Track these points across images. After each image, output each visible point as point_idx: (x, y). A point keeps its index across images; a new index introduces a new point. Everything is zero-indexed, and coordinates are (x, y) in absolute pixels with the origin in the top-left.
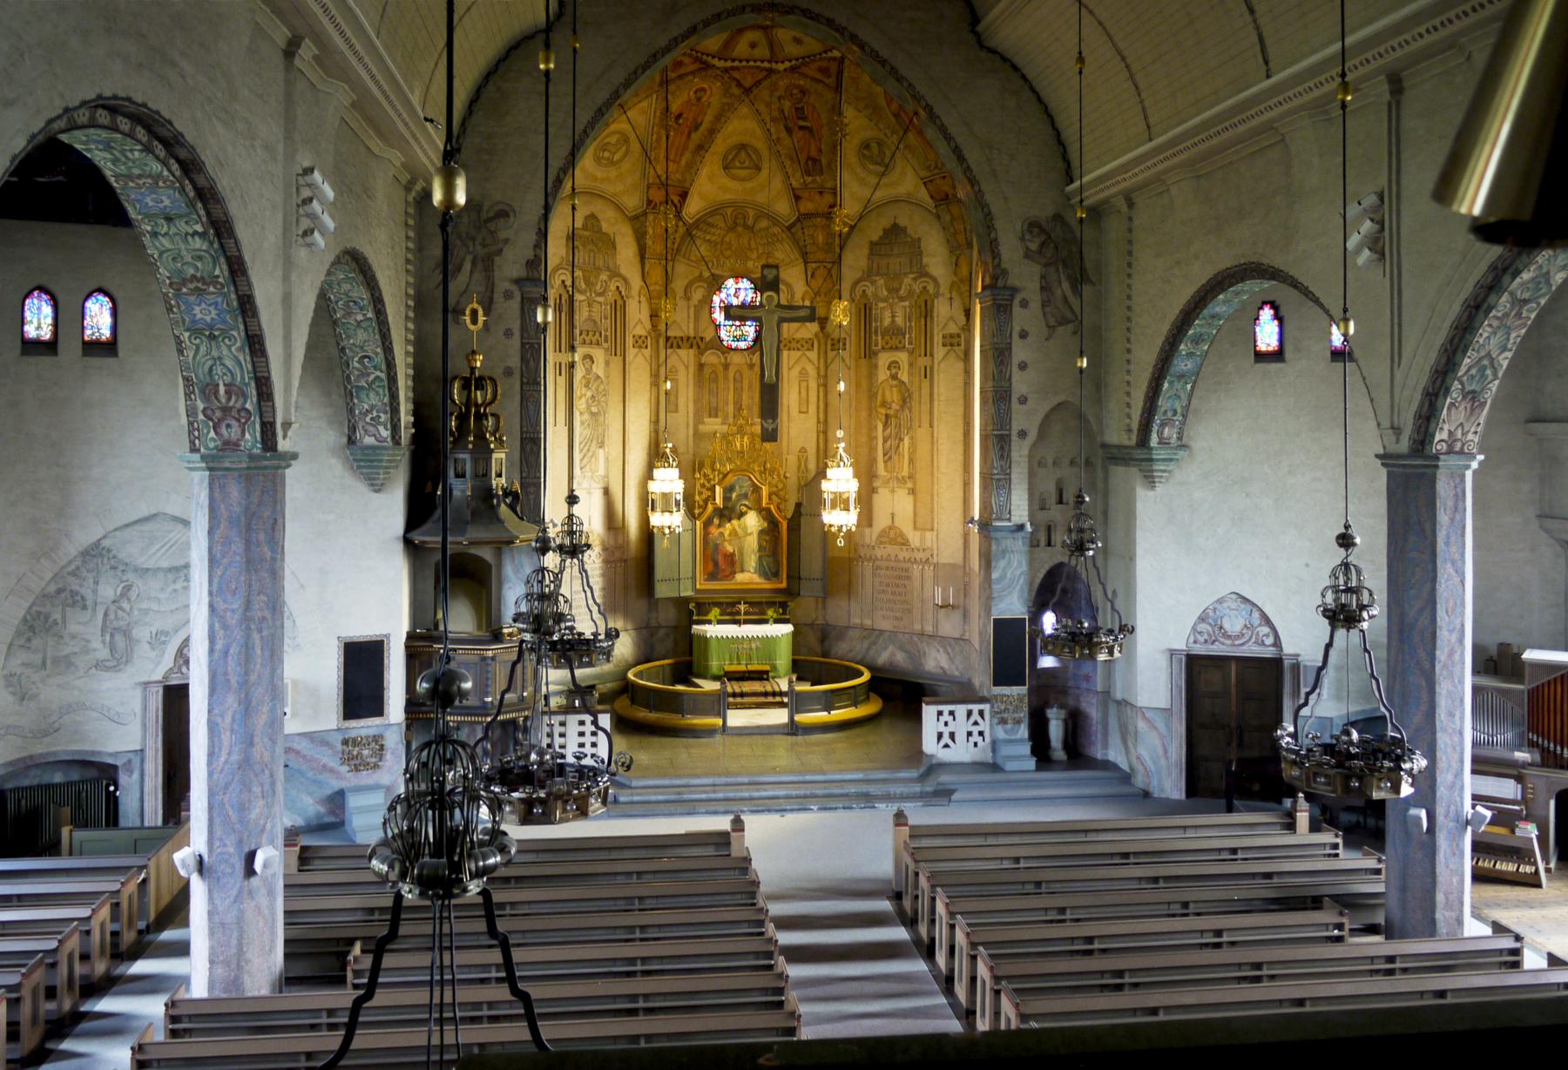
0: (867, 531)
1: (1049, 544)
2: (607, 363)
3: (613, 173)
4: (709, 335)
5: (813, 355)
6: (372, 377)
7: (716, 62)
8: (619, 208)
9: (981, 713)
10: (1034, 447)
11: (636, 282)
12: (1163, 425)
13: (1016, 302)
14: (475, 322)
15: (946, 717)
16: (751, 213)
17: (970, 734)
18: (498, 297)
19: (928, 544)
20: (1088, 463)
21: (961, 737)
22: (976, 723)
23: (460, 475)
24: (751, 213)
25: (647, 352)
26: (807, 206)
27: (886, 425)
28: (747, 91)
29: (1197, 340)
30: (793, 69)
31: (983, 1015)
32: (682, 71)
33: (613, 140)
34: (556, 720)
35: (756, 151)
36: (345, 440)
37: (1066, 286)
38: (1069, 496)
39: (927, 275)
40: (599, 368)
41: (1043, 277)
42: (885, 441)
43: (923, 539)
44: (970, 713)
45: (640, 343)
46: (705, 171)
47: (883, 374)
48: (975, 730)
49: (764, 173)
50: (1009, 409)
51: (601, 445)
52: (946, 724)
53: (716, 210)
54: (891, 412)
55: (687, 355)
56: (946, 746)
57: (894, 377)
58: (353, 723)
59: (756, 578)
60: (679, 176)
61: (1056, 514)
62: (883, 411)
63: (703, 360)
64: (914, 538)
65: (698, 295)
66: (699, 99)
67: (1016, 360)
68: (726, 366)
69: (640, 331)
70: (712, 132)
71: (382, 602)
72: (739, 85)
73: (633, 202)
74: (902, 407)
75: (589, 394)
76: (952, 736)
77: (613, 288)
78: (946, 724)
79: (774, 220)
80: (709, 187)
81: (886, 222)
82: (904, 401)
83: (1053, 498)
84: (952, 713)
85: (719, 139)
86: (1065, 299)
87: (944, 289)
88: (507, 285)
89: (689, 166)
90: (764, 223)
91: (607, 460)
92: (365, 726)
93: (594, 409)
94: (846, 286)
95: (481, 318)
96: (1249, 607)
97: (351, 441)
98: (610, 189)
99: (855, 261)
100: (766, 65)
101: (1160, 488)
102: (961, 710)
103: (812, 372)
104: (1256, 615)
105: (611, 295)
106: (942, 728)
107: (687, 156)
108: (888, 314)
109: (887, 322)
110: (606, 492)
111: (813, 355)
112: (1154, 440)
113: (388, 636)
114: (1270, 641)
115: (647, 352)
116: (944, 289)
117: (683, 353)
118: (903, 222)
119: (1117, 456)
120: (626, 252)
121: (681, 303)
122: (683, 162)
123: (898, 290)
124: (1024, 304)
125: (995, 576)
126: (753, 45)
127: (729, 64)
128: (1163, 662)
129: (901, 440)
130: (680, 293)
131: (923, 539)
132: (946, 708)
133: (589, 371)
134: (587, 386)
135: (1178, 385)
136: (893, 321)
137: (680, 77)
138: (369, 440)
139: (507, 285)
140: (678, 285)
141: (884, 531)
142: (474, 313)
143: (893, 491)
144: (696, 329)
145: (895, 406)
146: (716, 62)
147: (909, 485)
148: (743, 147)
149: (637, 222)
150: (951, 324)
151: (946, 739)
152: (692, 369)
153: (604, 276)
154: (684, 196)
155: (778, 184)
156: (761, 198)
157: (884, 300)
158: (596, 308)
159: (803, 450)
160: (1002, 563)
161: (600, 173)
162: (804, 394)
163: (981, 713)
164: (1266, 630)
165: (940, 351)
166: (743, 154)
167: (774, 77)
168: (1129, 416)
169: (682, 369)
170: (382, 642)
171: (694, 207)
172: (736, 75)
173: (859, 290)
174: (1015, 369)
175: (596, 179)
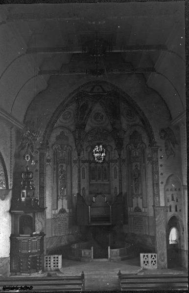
0: (132, 208)
4: (92, 159)
8: (69, 130)
9: (155, 256)
10: (165, 186)
13: (159, 150)
14: (28, 159)
15: (146, 257)
17: (152, 261)
20: (179, 189)
21: (150, 262)
22: (153, 259)
23: (23, 196)
25: (77, 164)
27: (135, 181)
33: (67, 113)
38: (175, 199)
39: (143, 143)
40: (64, 168)
41: (165, 143)
43: (145, 210)
44: (152, 256)
45: (75, 162)
47: (134, 168)
48: (154, 260)
50: (158, 177)
52: (146, 259)
56: (146, 265)
61: (171, 203)
65: (89, 149)
67: (159, 164)
75: (62, 175)
76: (148, 262)
78: (146, 259)
79: (69, 130)
83: (170, 199)
84: (147, 256)
86: (171, 148)
91: (67, 191)
94: (124, 146)
95: (29, 158)
102: (150, 255)
103: (117, 168)
106: (145, 260)
109: (134, 155)
115: (77, 164)
116: (147, 146)
117: (86, 164)
121: (85, 152)
123: (136, 147)
124: (161, 150)
126: (98, 89)
127: (93, 94)
130: (85, 149)
131: (145, 210)
132: (146, 255)
134: (62, 173)
136: (136, 155)
140: (84, 147)
142: (28, 157)
144: (89, 158)
147: (141, 196)
151: (146, 263)
153: (66, 146)
158: (63, 153)
159: (116, 188)
161: (64, 121)
163: (155, 256)
165: (147, 162)
174: (159, 166)
175: (63, 123)
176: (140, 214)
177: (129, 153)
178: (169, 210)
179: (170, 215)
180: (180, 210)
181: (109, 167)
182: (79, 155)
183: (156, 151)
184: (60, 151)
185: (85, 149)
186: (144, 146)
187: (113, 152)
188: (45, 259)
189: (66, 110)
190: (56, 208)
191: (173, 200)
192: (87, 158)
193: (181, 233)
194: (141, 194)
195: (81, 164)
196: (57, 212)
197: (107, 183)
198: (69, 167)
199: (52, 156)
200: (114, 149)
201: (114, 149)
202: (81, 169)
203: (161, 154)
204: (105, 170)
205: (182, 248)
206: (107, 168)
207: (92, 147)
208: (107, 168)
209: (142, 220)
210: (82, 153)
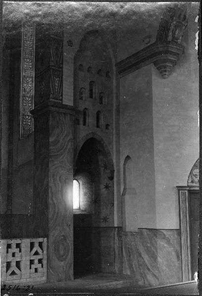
1: (84, 124)
12: (176, 27)
22: (36, 253)
44: (32, 245)
52: (14, 255)
78: (14, 255)
83: (86, 94)
84: (18, 246)
128: (174, 197)
160: (57, 131)
163: (40, 244)
178: (81, 122)
179: (84, 133)
180: (107, 126)
191: (91, 96)
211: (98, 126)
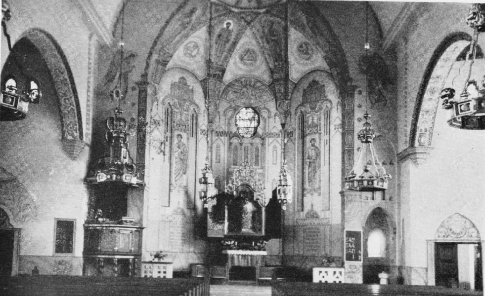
0: (301, 213)
2: (188, 139)
3: (192, 61)
5: (279, 140)
6: (69, 109)
7: (233, 9)
9: (341, 273)
11: (203, 107)
13: (356, 92)
15: (323, 274)
16: (253, 80)
18: (129, 90)
19: (327, 217)
22: (338, 277)
24: (253, 80)
26: (276, 76)
27: (309, 167)
28: (249, 23)
29: (433, 92)
30: (267, 12)
31: (98, 24)
32: (220, 13)
33: (192, 45)
34: (148, 266)
35: (254, 52)
36: (60, 138)
37: (380, 86)
39: (327, 100)
40: (184, 140)
42: (309, 174)
46: (232, 61)
49: (258, 62)
50: (353, 138)
51: (185, 173)
52: (323, 277)
53: (238, 80)
54: (312, 161)
55: (225, 139)
57: (313, 145)
58: (59, 254)
59: (251, 231)
60: (220, 63)
62: (308, 160)
63: (231, 141)
64: (322, 215)
65: (230, 114)
66: (228, 27)
67: (356, 117)
68: (241, 144)
69: (204, 128)
70: (235, 43)
71: (75, 205)
72: (245, 21)
73: (201, 74)
74: (316, 158)
75: (180, 151)
77: (192, 109)
78: (323, 277)
80: (235, 69)
81: (311, 79)
82: (317, 155)
84: (326, 272)
85: (238, 47)
87: (335, 104)
88: (134, 85)
89: (226, 58)
90: (258, 84)
92: (64, 256)
93: (182, 158)
96: (464, 220)
97: (63, 138)
98: (191, 68)
99: (298, 97)
100: (256, 10)
101: (420, 166)
104: (468, 223)
105: (191, 112)
107: (225, 54)
108: (311, 118)
110: (187, 193)
111: (279, 140)
112: (417, 144)
113: (75, 220)
114: (475, 234)
116: (335, 104)
117: (223, 138)
118: (317, 79)
119: (404, 157)
120: (199, 97)
121: (223, 118)
122: (223, 57)
124: (360, 93)
125: (346, 212)
129: (316, 172)
130: (222, 113)
133: (180, 141)
135: (426, 116)
137: (220, 16)
138: (69, 137)
139: (134, 85)
140: (221, 110)
141: (308, 213)
143: (312, 195)
145: (313, 158)
146: (233, 9)
148: (248, 51)
149: (204, 82)
150: (471, 89)
152: (226, 145)
153: (187, 103)
154: (223, 71)
155: (264, 67)
156: (257, 74)
157: (309, 113)
162: (275, 155)
163: (341, 273)
164: (473, 230)
166: (249, 53)
167: (260, 17)
168: (406, 136)
169: (222, 145)
170: (73, 222)
171: (228, 77)
172: (243, 16)
173: (299, 111)
174: (356, 121)
176: (316, 222)
177: (303, 120)
181: (263, 145)
182: (210, 122)
183: (352, 95)
184: (177, 111)
185: (222, 113)
186: (329, 105)
187: (272, 120)
188: (143, 270)
189: (190, 39)
190: (167, 205)
192: (224, 128)
193: (391, 239)
194: (320, 188)
195: (215, 138)
196: (169, 211)
197: (261, 171)
198: (193, 140)
199: (162, 116)
200: (273, 114)
201: (273, 114)
202: (214, 145)
203: (358, 99)
204: (257, 149)
205: (391, 265)
206: (260, 147)
207: (235, 110)
208: (260, 147)
209: (319, 232)
210: (217, 119)
211: (384, 199)
